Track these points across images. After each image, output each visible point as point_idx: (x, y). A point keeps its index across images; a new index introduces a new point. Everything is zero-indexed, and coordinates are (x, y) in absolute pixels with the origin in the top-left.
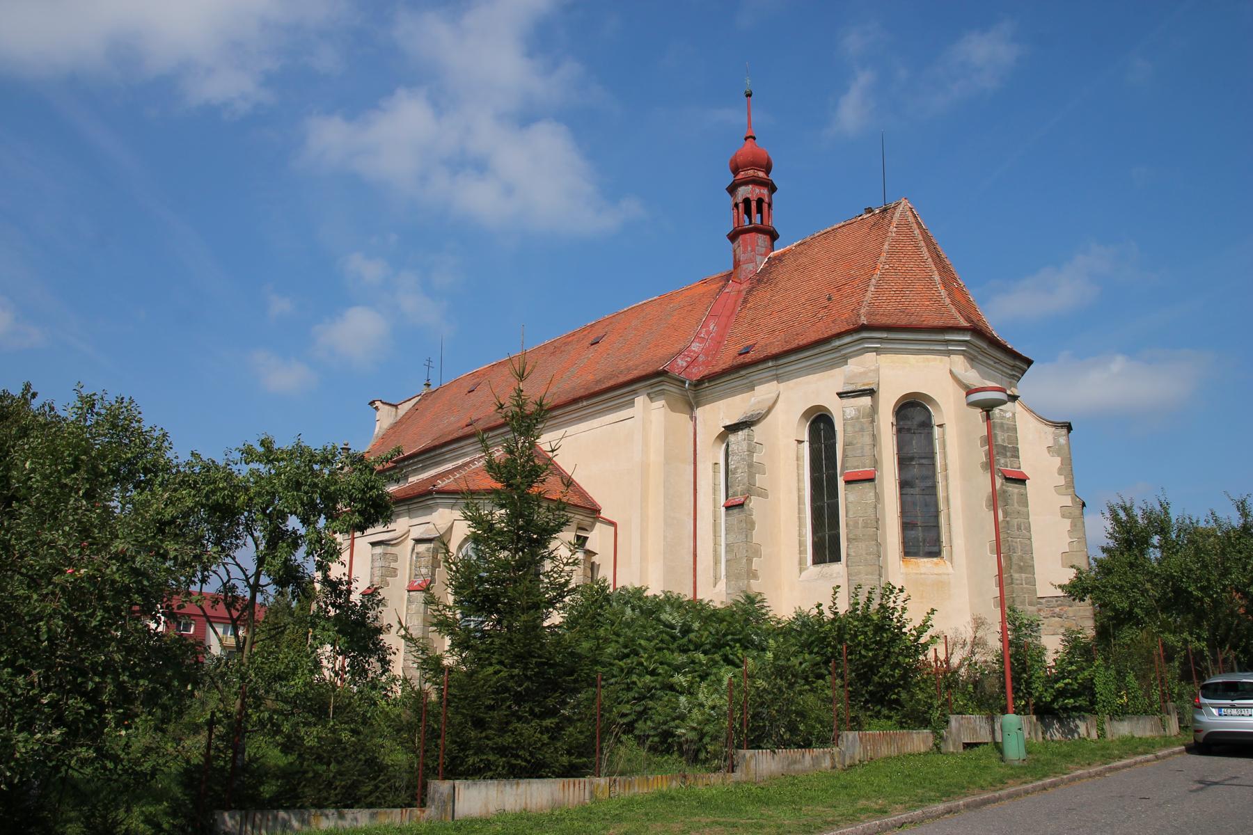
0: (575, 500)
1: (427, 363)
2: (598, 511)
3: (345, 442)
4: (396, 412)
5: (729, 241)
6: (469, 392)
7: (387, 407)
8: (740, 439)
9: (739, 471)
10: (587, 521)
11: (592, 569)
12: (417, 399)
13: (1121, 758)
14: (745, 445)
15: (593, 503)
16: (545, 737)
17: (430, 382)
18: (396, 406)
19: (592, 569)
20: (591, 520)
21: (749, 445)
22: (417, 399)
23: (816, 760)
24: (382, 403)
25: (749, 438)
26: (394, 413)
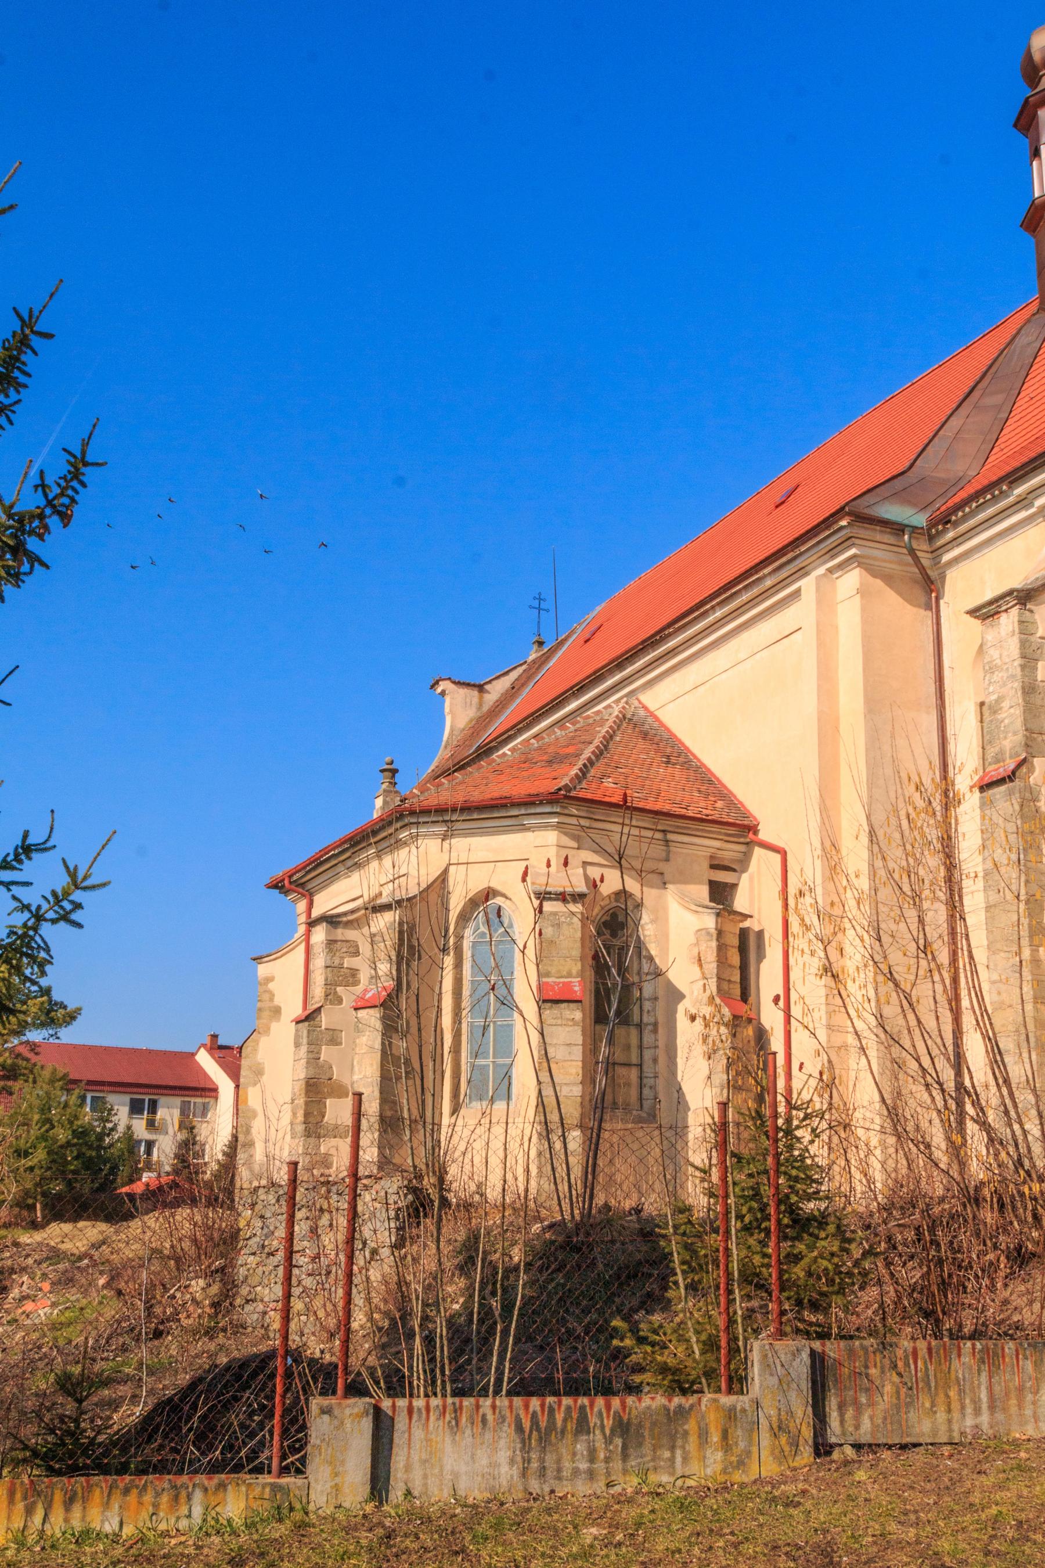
0: (698, 806)
1: (536, 603)
2: (753, 829)
3: (388, 759)
4: (481, 698)
5: (1026, 235)
6: (586, 642)
7: (463, 691)
8: (1003, 633)
9: (1005, 704)
10: (730, 851)
11: (743, 949)
12: (520, 670)
13: (469, 1082)
14: (1013, 647)
15: (747, 814)
16: (266, 1243)
17: (543, 638)
18: (480, 688)
19: (743, 949)
20: (742, 848)
21: (1023, 644)
22: (520, 670)
23: (145, 1227)
24: (454, 682)
25: (1025, 628)
26: (475, 700)
